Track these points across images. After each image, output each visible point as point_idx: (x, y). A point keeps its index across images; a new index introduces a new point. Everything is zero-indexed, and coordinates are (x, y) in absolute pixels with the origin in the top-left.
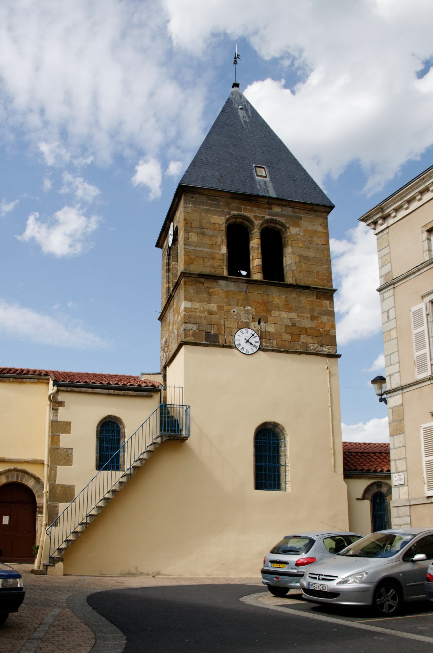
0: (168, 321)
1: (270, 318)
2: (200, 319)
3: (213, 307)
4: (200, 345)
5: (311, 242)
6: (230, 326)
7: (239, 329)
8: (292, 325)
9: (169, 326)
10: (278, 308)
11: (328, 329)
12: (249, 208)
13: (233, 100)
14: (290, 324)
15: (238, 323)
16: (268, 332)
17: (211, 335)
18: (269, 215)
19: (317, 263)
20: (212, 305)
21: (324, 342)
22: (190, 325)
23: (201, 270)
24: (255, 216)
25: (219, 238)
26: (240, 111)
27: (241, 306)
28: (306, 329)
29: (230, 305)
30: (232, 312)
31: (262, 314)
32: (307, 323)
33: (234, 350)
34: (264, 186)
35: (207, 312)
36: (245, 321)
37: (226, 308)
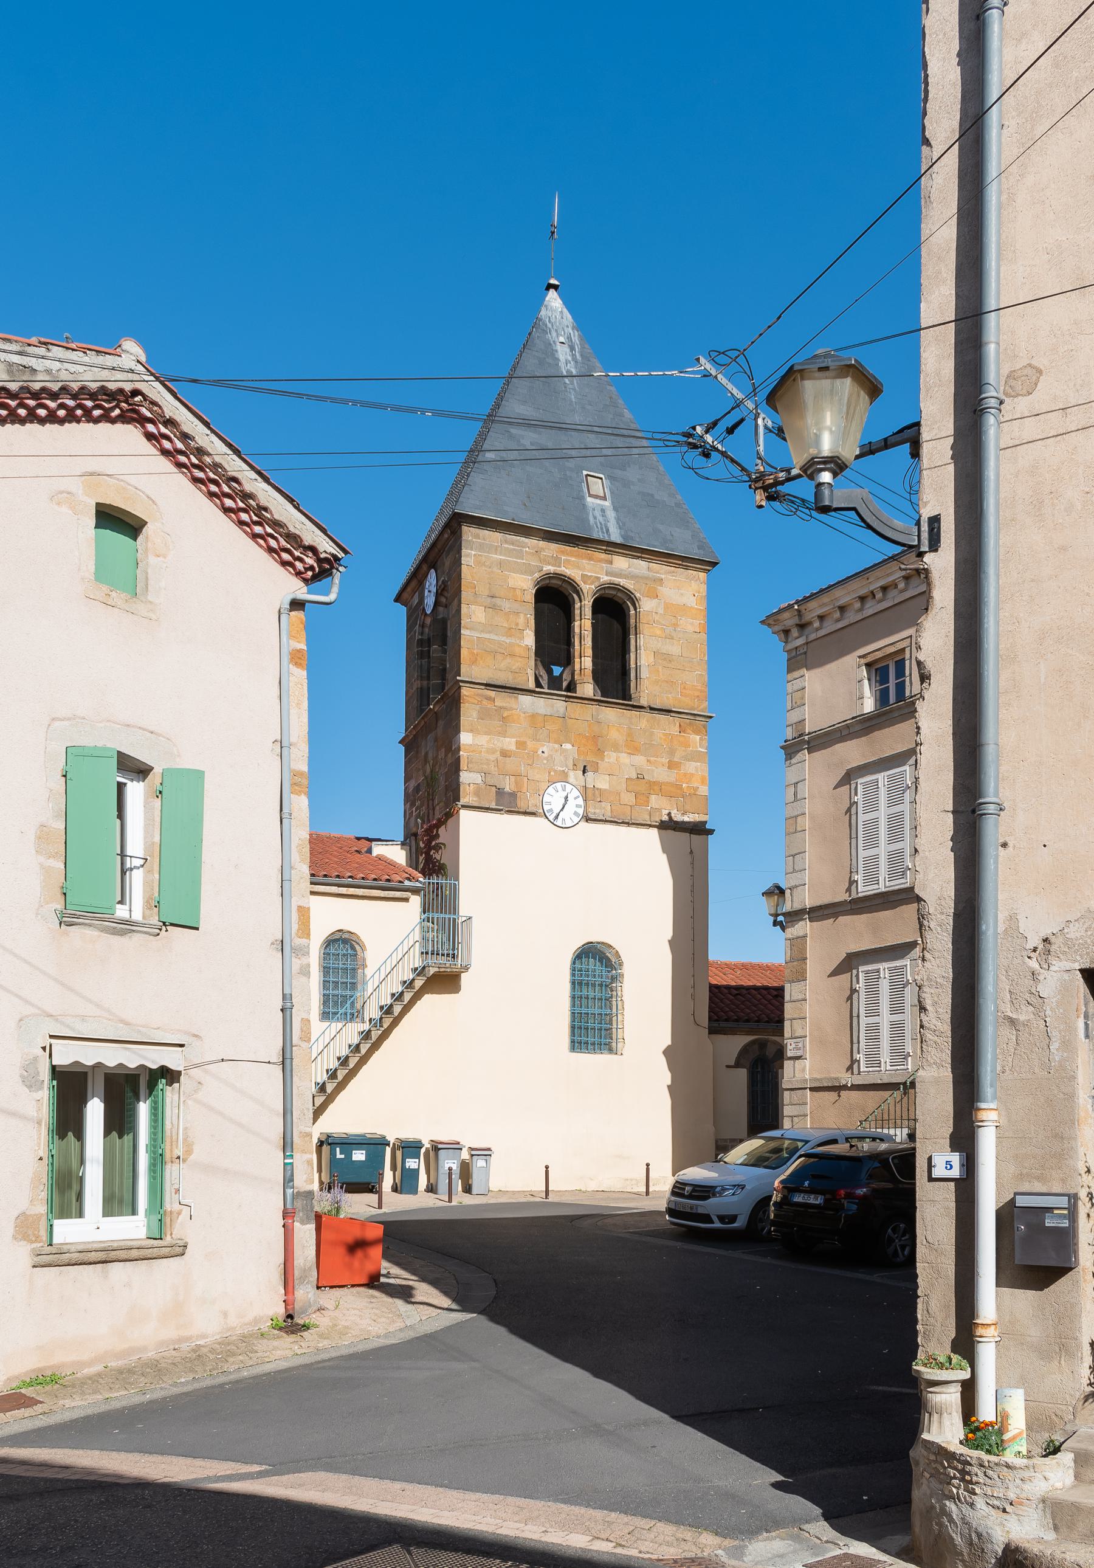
1: (602, 765)
3: (510, 743)
5: (675, 625)
6: (537, 778)
10: (616, 748)
14: (635, 776)
21: (687, 807)
25: (522, 615)
29: (538, 740)
32: (661, 774)
33: (540, 821)
37: (530, 744)
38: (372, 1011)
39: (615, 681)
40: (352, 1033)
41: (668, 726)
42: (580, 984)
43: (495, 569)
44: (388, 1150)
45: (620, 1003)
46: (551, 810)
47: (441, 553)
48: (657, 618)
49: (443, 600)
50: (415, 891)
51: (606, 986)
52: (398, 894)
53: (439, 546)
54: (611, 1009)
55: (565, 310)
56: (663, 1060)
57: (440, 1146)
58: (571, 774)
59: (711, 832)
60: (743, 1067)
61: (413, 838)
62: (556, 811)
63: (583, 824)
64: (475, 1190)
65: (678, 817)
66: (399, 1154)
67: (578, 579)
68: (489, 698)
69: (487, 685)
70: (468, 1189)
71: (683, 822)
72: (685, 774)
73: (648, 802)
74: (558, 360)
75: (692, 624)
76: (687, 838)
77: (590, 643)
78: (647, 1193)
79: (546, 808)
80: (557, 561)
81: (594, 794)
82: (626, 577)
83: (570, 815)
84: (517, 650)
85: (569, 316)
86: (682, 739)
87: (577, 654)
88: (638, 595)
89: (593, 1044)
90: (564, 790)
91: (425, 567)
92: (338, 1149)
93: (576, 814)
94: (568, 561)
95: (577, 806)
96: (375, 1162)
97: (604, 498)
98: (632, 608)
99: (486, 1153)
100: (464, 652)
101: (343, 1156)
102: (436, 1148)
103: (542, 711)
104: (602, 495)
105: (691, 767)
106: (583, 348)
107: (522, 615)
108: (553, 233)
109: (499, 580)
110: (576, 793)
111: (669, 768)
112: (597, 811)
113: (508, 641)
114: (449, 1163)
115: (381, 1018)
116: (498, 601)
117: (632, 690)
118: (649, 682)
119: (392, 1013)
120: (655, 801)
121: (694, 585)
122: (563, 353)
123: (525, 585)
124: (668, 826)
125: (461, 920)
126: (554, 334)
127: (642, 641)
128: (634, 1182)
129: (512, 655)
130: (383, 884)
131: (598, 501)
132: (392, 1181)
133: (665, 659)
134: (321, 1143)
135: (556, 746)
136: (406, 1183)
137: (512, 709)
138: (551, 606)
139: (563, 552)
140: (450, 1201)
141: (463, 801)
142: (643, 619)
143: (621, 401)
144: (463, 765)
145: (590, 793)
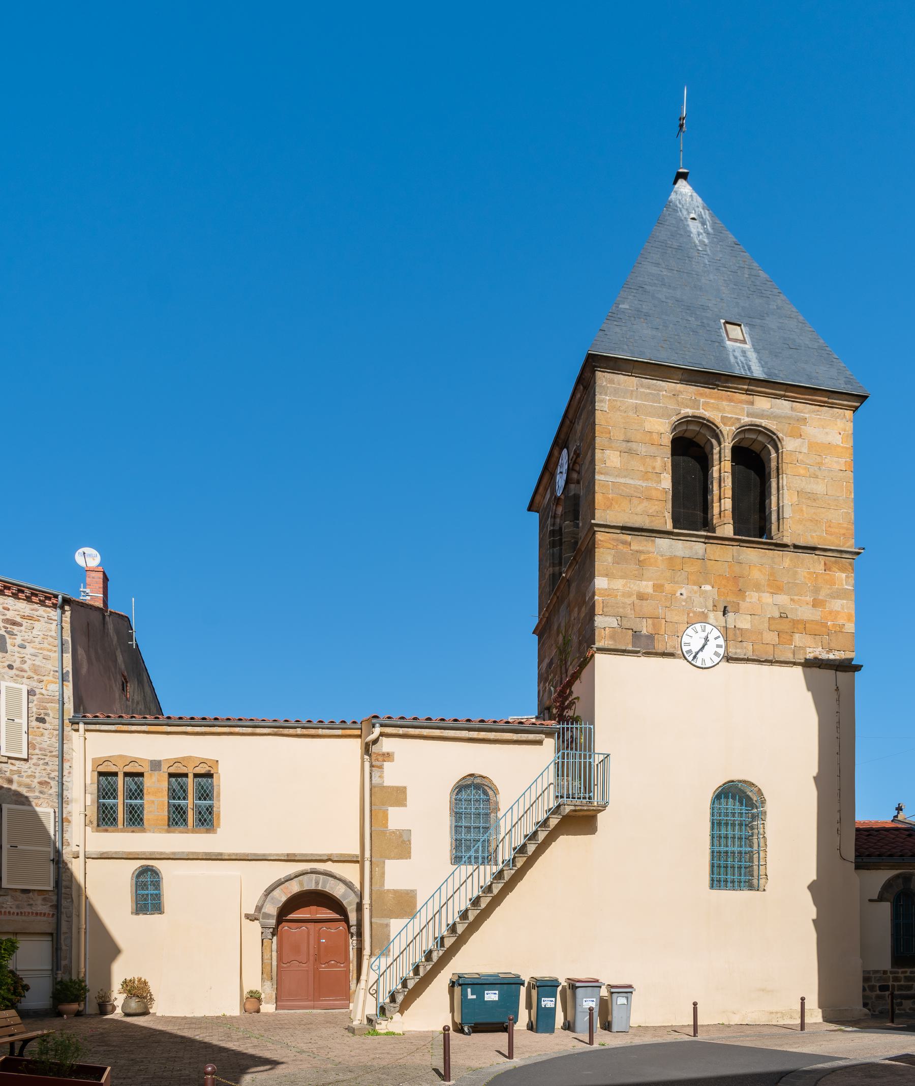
1: (743, 605)
2: (624, 608)
3: (646, 587)
4: (624, 652)
5: (820, 465)
6: (675, 619)
7: (690, 624)
9: (558, 635)
10: (758, 587)
11: (841, 622)
14: (777, 615)
15: (688, 614)
17: (641, 635)
18: (748, 416)
20: (644, 583)
21: (833, 645)
22: (607, 619)
23: (627, 520)
24: (722, 417)
25: (659, 459)
26: (690, 222)
27: (694, 584)
28: (805, 623)
30: (678, 594)
32: (805, 612)
33: (682, 662)
34: (743, 359)
37: (668, 587)
38: (505, 853)
39: (756, 521)
40: (486, 873)
41: (813, 564)
42: (719, 824)
43: (631, 414)
44: (523, 990)
45: (762, 841)
46: (690, 651)
47: (575, 433)
48: (800, 457)
49: (575, 476)
50: (549, 734)
51: (746, 825)
52: (531, 737)
53: (570, 416)
54: (751, 847)
55: (695, 194)
56: (808, 895)
57: (578, 984)
58: (711, 615)
59: (858, 668)
60: (887, 901)
62: (695, 650)
63: (724, 664)
64: (615, 1028)
65: (824, 656)
66: (534, 993)
67: (718, 421)
68: (625, 543)
70: (607, 1026)
71: (828, 660)
72: (831, 612)
73: (791, 640)
74: (691, 232)
75: (838, 462)
76: (833, 677)
77: (730, 484)
78: (803, 1026)
79: (685, 649)
80: (695, 404)
81: (735, 635)
82: (768, 417)
83: (708, 656)
84: (654, 494)
85: (699, 200)
86: (827, 577)
87: (716, 498)
88: (780, 435)
89: (733, 882)
90: (704, 631)
91: (556, 453)
92: (469, 990)
93: (716, 654)
94: (708, 403)
95: (718, 646)
96: (509, 1003)
97: (744, 342)
99: (627, 990)
100: (598, 498)
101: (474, 997)
102: (573, 986)
103: (680, 553)
104: (742, 338)
105: (837, 605)
106: (714, 223)
107: (659, 459)
108: (681, 126)
109: (635, 424)
110: (716, 633)
111: (814, 606)
112: (738, 651)
113: (644, 485)
114: (588, 1002)
115: (515, 857)
116: (634, 446)
117: (774, 527)
119: (526, 852)
120: (798, 639)
121: (840, 424)
122: (695, 228)
123: (662, 429)
125: (598, 759)
126: (685, 213)
127: (784, 481)
128: (779, 1015)
129: (649, 499)
130: (517, 733)
131: (738, 344)
132: (527, 1020)
133: (809, 498)
134: (453, 984)
135: (696, 588)
136: (542, 1022)
137: (648, 552)
138: (686, 458)
139: (701, 395)
140: (591, 1042)
141: (599, 644)
142: (786, 458)
143: (755, 264)
144: (598, 610)
145: (730, 633)
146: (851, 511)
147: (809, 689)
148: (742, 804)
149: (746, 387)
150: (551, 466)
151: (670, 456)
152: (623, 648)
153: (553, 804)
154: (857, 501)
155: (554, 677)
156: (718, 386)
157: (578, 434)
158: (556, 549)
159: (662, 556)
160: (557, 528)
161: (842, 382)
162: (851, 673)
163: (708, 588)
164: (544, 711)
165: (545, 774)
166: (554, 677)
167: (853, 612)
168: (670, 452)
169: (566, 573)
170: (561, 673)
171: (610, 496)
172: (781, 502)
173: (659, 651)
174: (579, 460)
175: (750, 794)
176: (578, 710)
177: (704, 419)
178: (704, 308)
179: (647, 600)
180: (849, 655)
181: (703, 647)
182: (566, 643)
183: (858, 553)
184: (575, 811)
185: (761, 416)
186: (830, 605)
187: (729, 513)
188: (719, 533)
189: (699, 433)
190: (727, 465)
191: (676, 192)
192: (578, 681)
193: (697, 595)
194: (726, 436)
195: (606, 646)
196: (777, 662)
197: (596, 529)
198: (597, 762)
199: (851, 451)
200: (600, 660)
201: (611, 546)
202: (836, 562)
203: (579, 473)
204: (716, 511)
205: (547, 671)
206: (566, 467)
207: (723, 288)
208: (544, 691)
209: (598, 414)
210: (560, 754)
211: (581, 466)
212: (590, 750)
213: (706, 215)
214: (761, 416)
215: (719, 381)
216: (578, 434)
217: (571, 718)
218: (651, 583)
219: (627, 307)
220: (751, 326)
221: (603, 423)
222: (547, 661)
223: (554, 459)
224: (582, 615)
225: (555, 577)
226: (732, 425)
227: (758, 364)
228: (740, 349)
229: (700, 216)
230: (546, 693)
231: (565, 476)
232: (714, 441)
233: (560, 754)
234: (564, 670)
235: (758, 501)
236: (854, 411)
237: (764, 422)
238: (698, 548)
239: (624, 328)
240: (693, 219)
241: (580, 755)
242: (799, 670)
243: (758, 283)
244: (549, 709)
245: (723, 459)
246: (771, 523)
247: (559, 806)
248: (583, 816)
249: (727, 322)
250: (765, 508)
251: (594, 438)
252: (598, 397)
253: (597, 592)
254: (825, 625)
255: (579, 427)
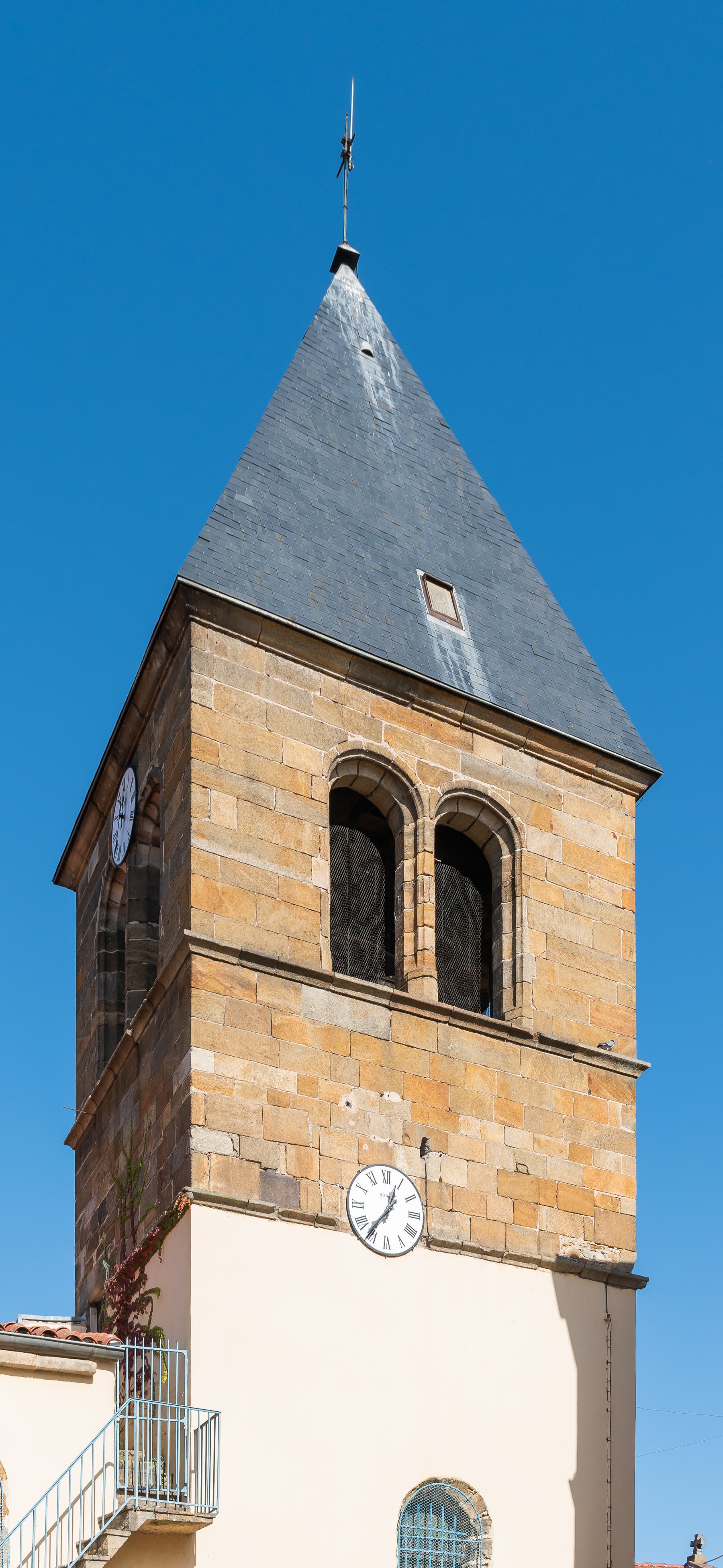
0: (111, 1140)
1: (455, 1141)
2: (245, 1118)
3: (285, 1080)
4: (244, 1207)
5: (582, 890)
6: (337, 1152)
7: (363, 1165)
8: (518, 1171)
9: (117, 1155)
10: (479, 1109)
11: (615, 1192)
12: (403, 729)
13: (339, 310)
14: (512, 1167)
15: (360, 1146)
16: (447, 1185)
17: (275, 1177)
18: (463, 771)
19: (596, 967)
20: (282, 1072)
21: (602, 1236)
22: (213, 1135)
23: (250, 940)
24: (421, 765)
25: (308, 826)
26: (362, 358)
27: (371, 1087)
28: (556, 1187)
29: (339, 1080)
30: (342, 1104)
31: (435, 1123)
32: (558, 1168)
33: (343, 1239)
34: (455, 656)
35: (265, 1096)
36: (382, 1140)
37: (324, 1086)
39: (477, 984)
43: (256, 723)
46: (364, 1219)
48: (551, 868)
49: (149, 828)
50: (105, 1362)
52: (70, 1364)
53: (141, 702)
55: (369, 303)
58: (401, 1153)
59: (639, 1283)
61: (93, 1310)
62: (373, 1217)
63: (421, 1251)
65: (588, 1254)
67: (412, 770)
69: (244, 955)
71: (594, 1262)
73: (535, 1218)
74: (362, 377)
75: (611, 890)
76: (600, 1285)
77: (433, 900)
79: (355, 1213)
80: (372, 728)
81: (440, 1196)
82: (497, 781)
83: (393, 1232)
84: (300, 895)
85: (378, 317)
86: (593, 1105)
87: (408, 923)
88: (518, 820)
90: (387, 1181)
91: (112, 772)
93: (409, 1229)
95: (411, 1215)
97: (457, 622)
98: (505, 849)
100: (197, 884)
104: (454, 616)
106: (403, 373)
107: (308, 826)
108: (345, 156)
109: (265, 742)
110: (407, 1189)
111: (571, 1157)
112: (447, 1228)
113: (282, 873)
117: (507, 996)
118: (540, 990)
122: (370, 370)
123: (313, 767)
124: (569, 1267)
125: (195, 1420)
126: (353, 336)
127: (525, 910)
129: (290, 903)
131: (447, 626)
135: (374, 1095)
139: (384, 712)
141: (198, 1185)
142: (528, 866)
143: (475, 474)
144: (197, 1115)
145: (433, 1191)
146: (632, 985)
147: (562, 1315)
148: (450, 1525)
149: (460, 713)
150: (102, 799)
151: (327, 823)
152: (244, 1199)
153: (111, 1505)
154: (640, 966)
155: (109, 1240)
156: (413, 700)
157: (157, 744)
158: (113, 974)
159: (314, 1022)
160: (113, 930)
161: (618, 738)
162: (630, 1290)
163: (394, 1097)
164: (89, 1310)
165: (99, 1443)
166: (109, 1240)
167: (634, 1177)
168: (327, 816)
169: (134, 1028)
170: (123, 1235)
171: (219, 885)
172: (518, 949)
173: (310, 1212)
174: (158, 798)
175: (465, 1506)
176: (156, 1316)
177: (388, 761)
178: (389, 540)
179: (286, 1106)
180: (628, 1257)
181: (386, 1214)
182: (134, 1173)
183: (643, 1068)
184: (155, 1522)
185: (486, 776)
186: (592, 1156)
187: (430, 956)
188: (414, 992)
189: (378, 787)
190: (428, 862)
191: (336, 288)
192: (155, 1258)
193: (377, 1109)
194: (426, 803)
195: (212, 1192)
196: (511, 1257)
197: (193, 948)
198: (195, 1425)
199: (632, 872)
200: (201, 1217)
201: (221, 988)
202: (607, 1079)
203: (157, 825)
204: (408, 948)
205: (94, 1228)
206: (130, 807)
207: (420, 506)
208: (89, 1267)
209: (196, 711)
210: (126, 1405)
211: (161, 814)
212: (182, 1402)
213: (391, 351)
214: (486, 776)
215: (415, 691)
216: (157, 744)
217: (143, 1329)
218: (293, 1074)
219: (250, 502)
220: (471, 596)
221: (205, 731)
222: (93, 1206)
223: (107, 785)
224: (166, 1121)
225: (110, 1034)
226: (437, 783)
227: (481, 673)
228: (449, 634)
229: (379, 348)
230: (93, 1274)
231: (129, 825)
232: (404, 808)
233: (126, 1405)
234: (128, 1230)
235: (478, 939)
236: (637, 798)
237: (491, 790)
238: (377, 1016)
239: (245, 545)
240: (367, 352)
241: (173, 1409)
242: (546, 1276)
243: (480, 512)
244: (98, 1305)
245: (420, 848)
246: (501, 987)
247: (124, 1512)
248: (169, 1534)
249: (428, 578)
250: (490, 957)
251: (188, 759)
252: (196, 677)
253: (194, 1078)
254: (588, 1195)
255: (157, 730)
